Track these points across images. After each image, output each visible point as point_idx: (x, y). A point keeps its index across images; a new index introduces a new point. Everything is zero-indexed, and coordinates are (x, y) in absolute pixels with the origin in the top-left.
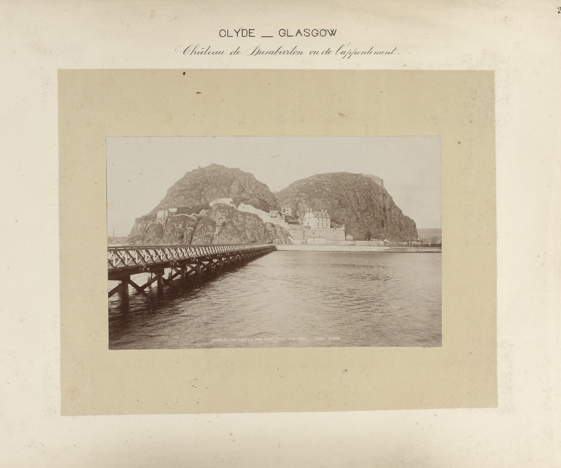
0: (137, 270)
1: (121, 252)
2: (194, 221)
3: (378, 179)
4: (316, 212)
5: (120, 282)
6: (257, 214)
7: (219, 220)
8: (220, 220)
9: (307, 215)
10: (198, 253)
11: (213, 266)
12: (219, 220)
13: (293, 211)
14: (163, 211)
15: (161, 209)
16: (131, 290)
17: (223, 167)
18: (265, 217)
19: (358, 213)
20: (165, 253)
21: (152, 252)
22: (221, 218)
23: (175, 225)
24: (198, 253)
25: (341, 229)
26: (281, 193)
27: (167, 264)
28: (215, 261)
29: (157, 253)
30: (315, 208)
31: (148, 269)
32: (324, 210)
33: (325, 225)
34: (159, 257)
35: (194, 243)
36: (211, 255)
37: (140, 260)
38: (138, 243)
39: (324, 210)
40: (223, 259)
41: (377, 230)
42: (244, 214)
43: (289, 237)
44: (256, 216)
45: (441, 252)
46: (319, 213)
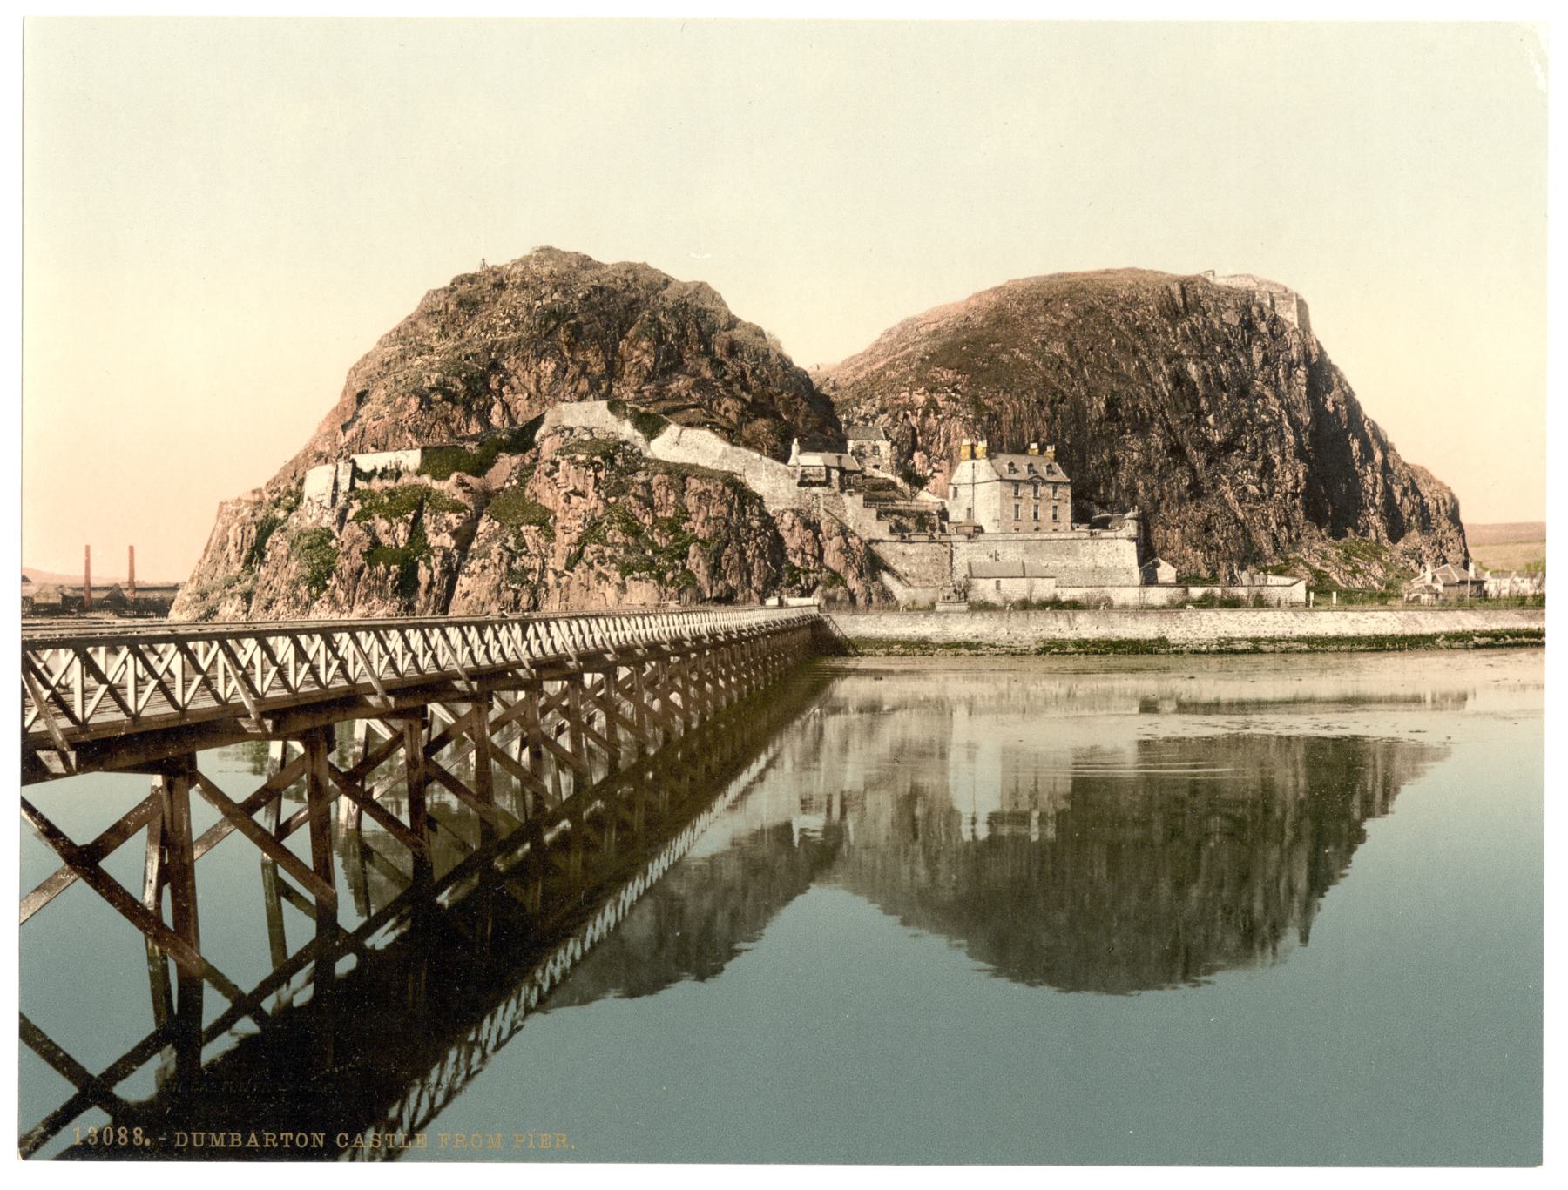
0: (220, 726)
1: (160, 648)
2: (457, 508)
3: (1287, 295)
4: (1004, 460)
5: (157, 780)
6: (736, 468)
7: (567, 500)
8: (575, 500)
9: (964, 471)
10: (480, 656)
11: (371, 759)
12: (567, 500)
13: (900, 454)
14: (330, 468)
15: (321, 458)
16: (202, 814)
17: (586, 263)
18: (772, 483)
19: (1198, 459)
20: (335, 651)
21: (283, 648)
22: (576, 493)
23: (382, 525)
24: (480, 656)
25: (1122, 533)
26: (846, 377)
27: (220, 726)
28: (553, 687)
29: (301, 655)
30: (1001, 440)
31: (269, 723)
32: (1042, 450)
33: (1046, 514)
34: (313, 670)
35: (457, 610)
36: (534, 663)
37: (234, 683)
38: (230, 611)
39: (1042, 450)
40: (588, 678)
41: (1283, 536)
42: (679, 474)
43: (886, 578)
44: (1197, 872)
45: (1534, 640)
46: (1022, 462)
